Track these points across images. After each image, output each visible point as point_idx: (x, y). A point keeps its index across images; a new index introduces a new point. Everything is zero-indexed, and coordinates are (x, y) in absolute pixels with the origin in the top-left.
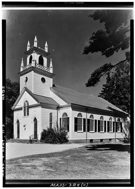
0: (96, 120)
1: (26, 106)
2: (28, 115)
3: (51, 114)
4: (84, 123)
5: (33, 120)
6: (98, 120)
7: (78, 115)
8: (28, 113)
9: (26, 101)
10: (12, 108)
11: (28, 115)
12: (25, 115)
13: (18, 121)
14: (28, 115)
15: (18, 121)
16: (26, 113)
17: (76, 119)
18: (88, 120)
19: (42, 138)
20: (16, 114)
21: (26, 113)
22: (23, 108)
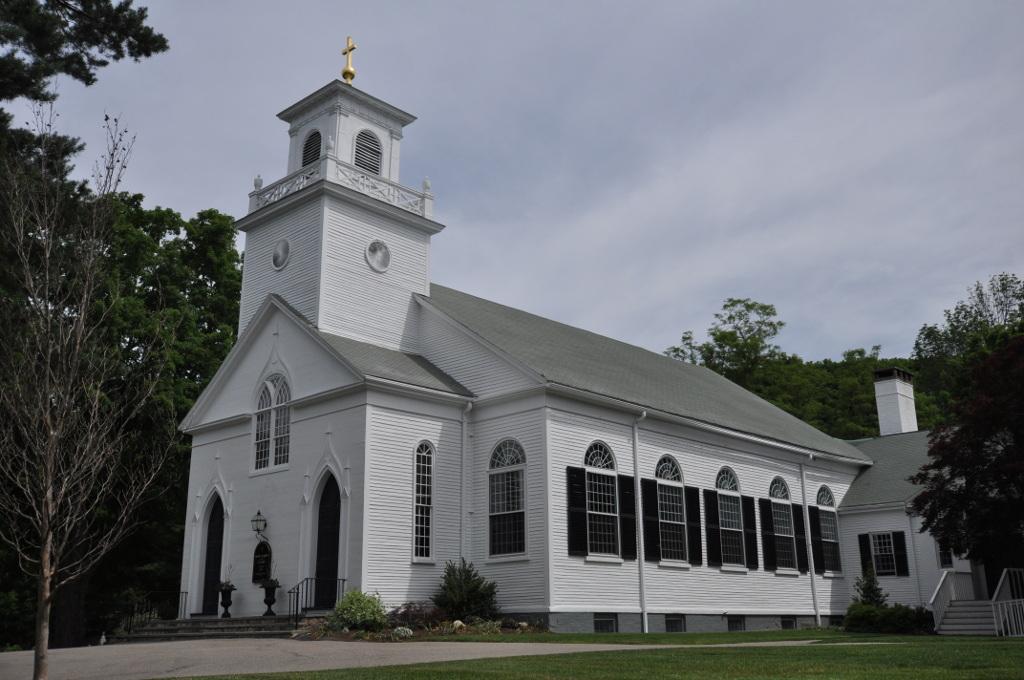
0: (696, 490)
1: (274, 405)
2: (282, 457)
3: (424, 447)
4: (1018, 592)
5: (310, 493)
6: (705, 491)
7: (587, 454)
8: (286, 450)
9: (275, 379)
10: (185, 426)
11: (285, 460)
12: (261, 461)
13: (216, 513)
14: (285, 460)
15: (216, 513)
16: (271, 450)
17: (575, 476)
18: (813, 511)
19: (250, 419)
20: (202, 460)
21: (271, 450)
22: (255, 419)
